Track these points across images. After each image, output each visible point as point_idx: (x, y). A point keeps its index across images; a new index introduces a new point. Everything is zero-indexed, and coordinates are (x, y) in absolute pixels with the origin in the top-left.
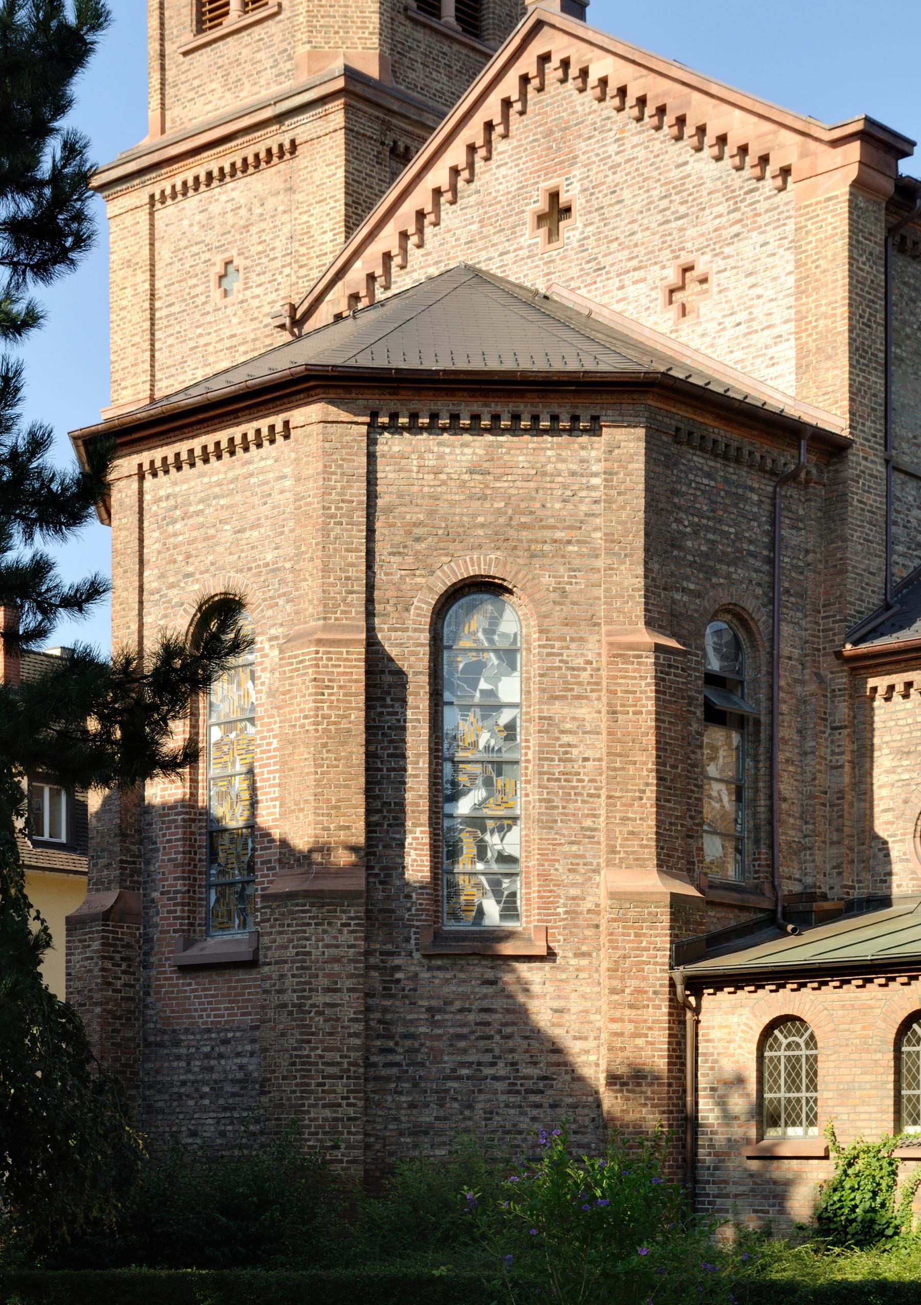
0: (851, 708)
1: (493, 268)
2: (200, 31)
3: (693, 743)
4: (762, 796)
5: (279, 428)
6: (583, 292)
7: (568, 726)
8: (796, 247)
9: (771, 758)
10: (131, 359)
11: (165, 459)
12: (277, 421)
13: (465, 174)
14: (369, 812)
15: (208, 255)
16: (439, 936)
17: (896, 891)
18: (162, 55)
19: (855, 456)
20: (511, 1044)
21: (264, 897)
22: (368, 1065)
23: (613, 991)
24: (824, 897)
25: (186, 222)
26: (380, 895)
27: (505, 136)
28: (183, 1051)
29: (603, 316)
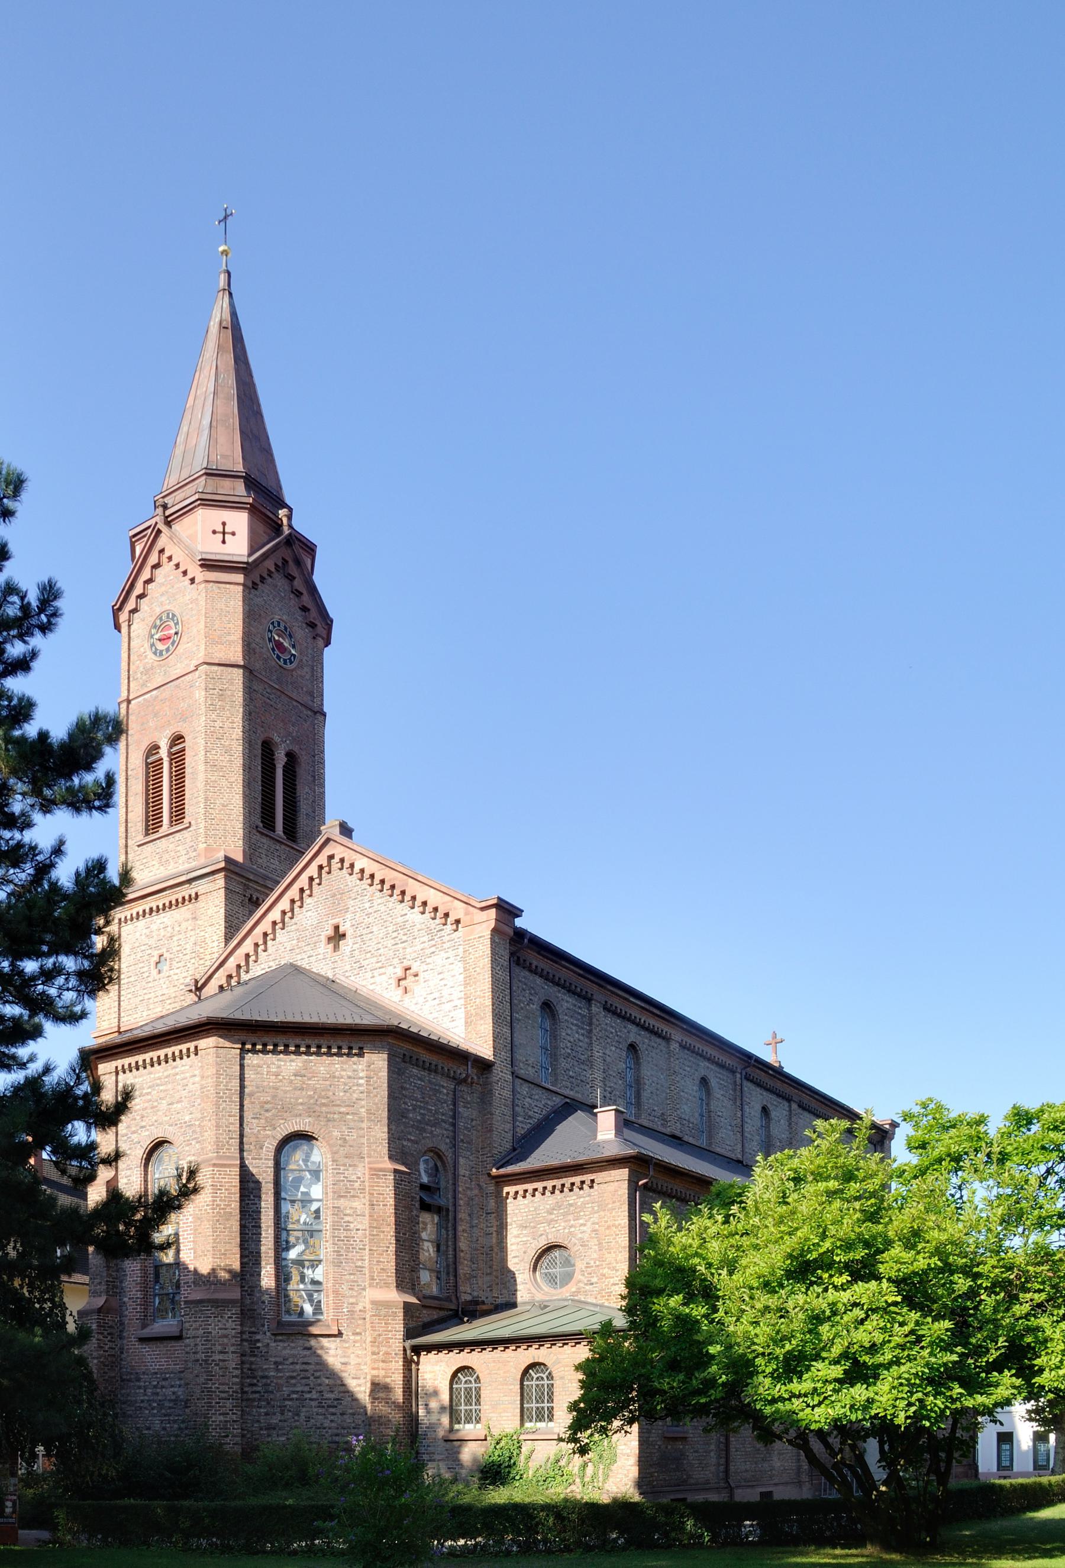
0: (496, 1202)
1: (304, 964)
2: (147, 834)
3: (414, 1221)
4: (450, 1249)
5: (192, 1049)
6: (352, 978)
7: (348, 1212)
8: (464, 960)
9: (455, 1229)
10: (107, 1006)
11: (130, 1064)
12: (191, 1045)
13: (289, 914)
14: (242, 1257)
15: (149, 951)
16: (280, 1324)
17: (519, 1300)
18: (126, 846)
19: (496, 1069)
20: (319, 1381)
21: (186, 1302)
22: (243, 1392)
23: (373, 1353)
24: (483, 1303)
25: (138, 934)
26: (248, 1302)
27: (310, 896)
28: (142, 1384)
29: (363, 991)
